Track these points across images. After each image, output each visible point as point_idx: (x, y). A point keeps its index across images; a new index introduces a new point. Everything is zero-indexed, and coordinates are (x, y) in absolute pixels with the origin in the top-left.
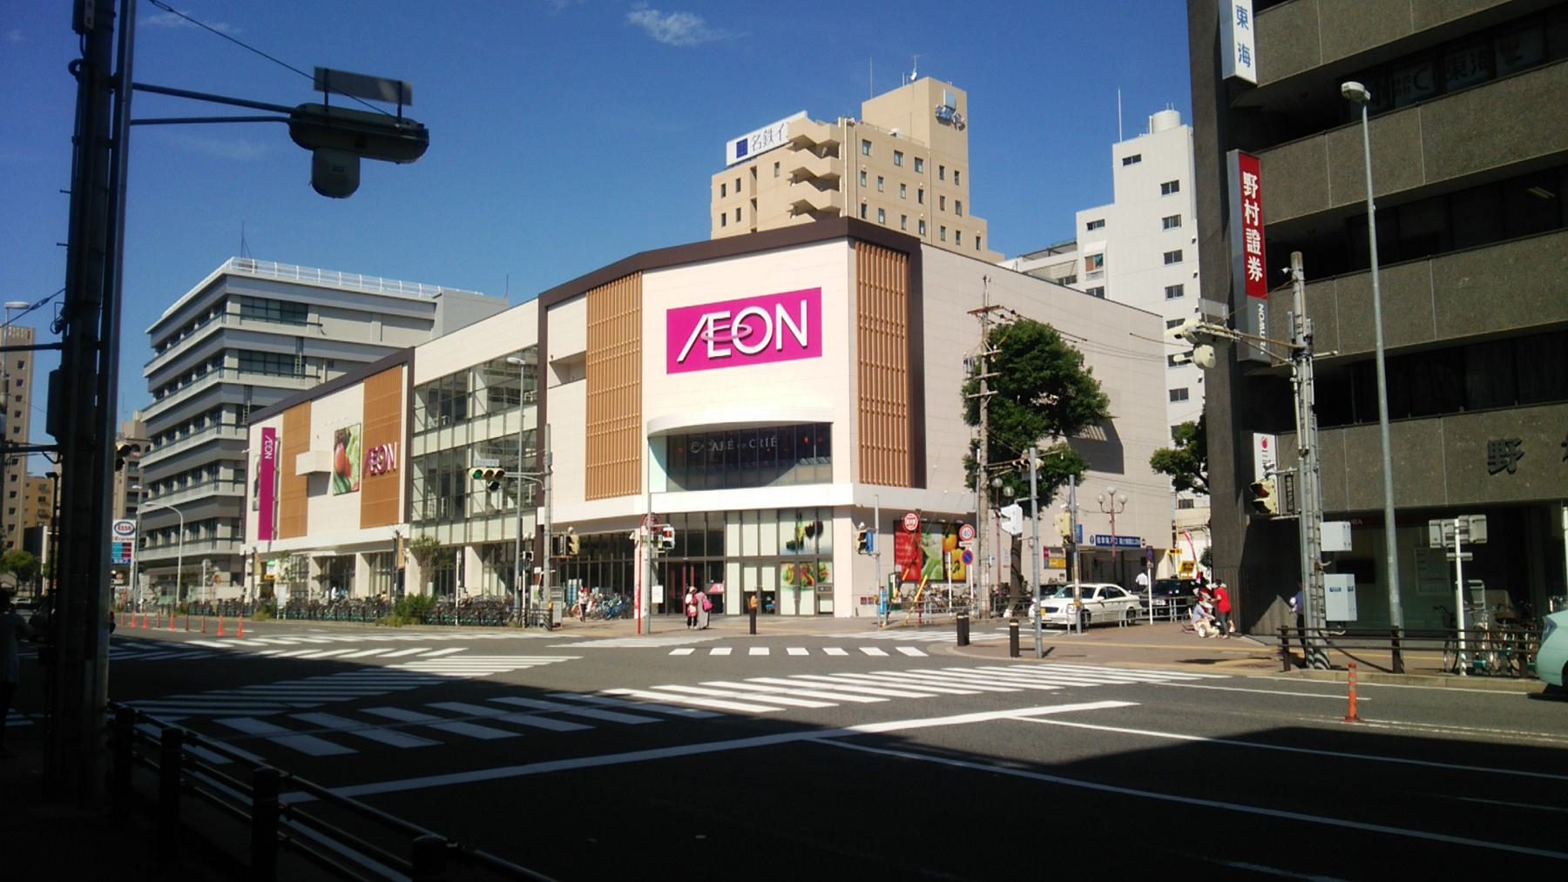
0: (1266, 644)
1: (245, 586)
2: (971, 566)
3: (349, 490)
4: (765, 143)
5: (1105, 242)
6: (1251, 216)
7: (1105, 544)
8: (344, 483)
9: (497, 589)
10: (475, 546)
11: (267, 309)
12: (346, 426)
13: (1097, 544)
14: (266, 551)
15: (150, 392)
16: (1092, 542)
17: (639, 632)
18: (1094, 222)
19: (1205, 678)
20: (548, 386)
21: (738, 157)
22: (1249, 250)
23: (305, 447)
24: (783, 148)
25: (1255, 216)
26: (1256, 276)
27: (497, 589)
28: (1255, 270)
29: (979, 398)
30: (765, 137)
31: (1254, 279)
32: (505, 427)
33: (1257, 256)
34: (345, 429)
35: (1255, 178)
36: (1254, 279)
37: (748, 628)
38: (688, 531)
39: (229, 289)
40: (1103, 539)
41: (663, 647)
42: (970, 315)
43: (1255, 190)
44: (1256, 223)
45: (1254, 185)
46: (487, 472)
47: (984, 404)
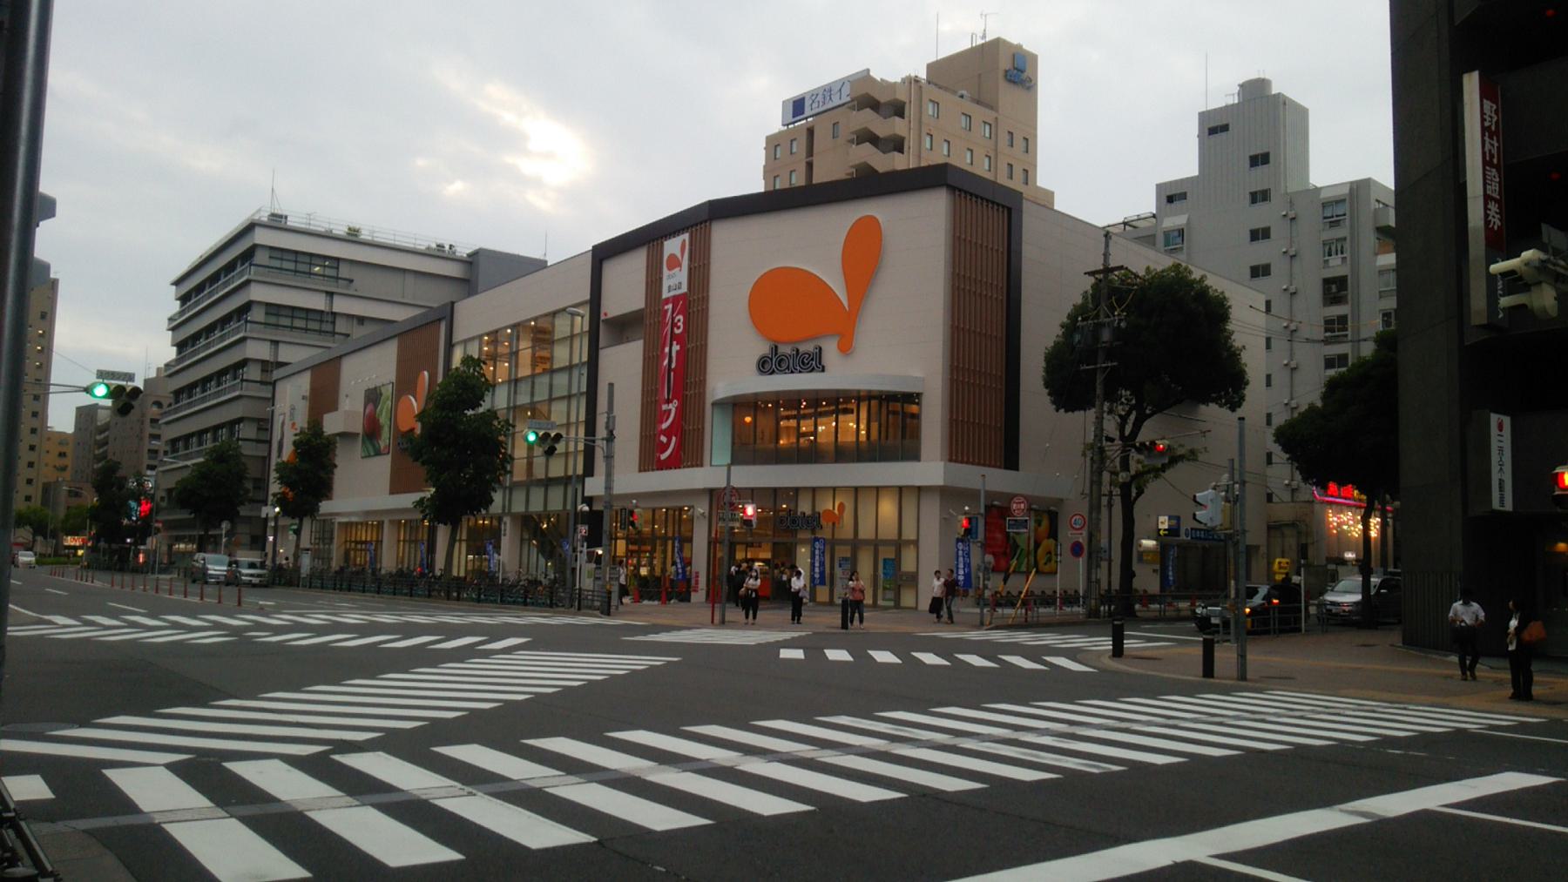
0: (1491, 668)
1: (267, 551)
2: (1081, 559)
3: (378, 453)
4: (824, 103)
5: (1186, 216)
6: (1490, 151)
7: (1200, 538)
8: (374, 446)
9: (542, 568)
10: (514, 516)
11: (296, 262)
12: (378, 385)
13: (1192, 538)
14: (563, 474)
15: (177, 299)
16: (1187, 535)
17: (713, 622)
18: (1175, 195)
19: (1522, 723)
20: (600, 346)
21: (794, 117)
22: (1488, 192)
23: (333, 406)
24: (844, 107)
25: (1495, 152)
26: (1494, 223)
27: (542, 568)
28: (1494, 217)
29: (1095, 369)
30: (824, 95)
31: (1493, 227)
32: (532, 394)
33: (1496, 201)
34: (376, 388)
35: (1495, 107)
36: (1493, 227)
37: (839, 622)
38: (987, 493)
39: (261, 237)
40: (1198, 532)
41: (769, 644)
42: (1087, 275)
43: (1494, 120)
44: (1495, 161)
45: (1493, 115)
46: (544, 434)
47: (1100, 378)
